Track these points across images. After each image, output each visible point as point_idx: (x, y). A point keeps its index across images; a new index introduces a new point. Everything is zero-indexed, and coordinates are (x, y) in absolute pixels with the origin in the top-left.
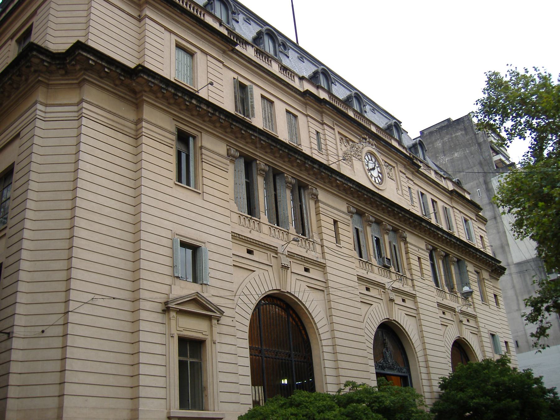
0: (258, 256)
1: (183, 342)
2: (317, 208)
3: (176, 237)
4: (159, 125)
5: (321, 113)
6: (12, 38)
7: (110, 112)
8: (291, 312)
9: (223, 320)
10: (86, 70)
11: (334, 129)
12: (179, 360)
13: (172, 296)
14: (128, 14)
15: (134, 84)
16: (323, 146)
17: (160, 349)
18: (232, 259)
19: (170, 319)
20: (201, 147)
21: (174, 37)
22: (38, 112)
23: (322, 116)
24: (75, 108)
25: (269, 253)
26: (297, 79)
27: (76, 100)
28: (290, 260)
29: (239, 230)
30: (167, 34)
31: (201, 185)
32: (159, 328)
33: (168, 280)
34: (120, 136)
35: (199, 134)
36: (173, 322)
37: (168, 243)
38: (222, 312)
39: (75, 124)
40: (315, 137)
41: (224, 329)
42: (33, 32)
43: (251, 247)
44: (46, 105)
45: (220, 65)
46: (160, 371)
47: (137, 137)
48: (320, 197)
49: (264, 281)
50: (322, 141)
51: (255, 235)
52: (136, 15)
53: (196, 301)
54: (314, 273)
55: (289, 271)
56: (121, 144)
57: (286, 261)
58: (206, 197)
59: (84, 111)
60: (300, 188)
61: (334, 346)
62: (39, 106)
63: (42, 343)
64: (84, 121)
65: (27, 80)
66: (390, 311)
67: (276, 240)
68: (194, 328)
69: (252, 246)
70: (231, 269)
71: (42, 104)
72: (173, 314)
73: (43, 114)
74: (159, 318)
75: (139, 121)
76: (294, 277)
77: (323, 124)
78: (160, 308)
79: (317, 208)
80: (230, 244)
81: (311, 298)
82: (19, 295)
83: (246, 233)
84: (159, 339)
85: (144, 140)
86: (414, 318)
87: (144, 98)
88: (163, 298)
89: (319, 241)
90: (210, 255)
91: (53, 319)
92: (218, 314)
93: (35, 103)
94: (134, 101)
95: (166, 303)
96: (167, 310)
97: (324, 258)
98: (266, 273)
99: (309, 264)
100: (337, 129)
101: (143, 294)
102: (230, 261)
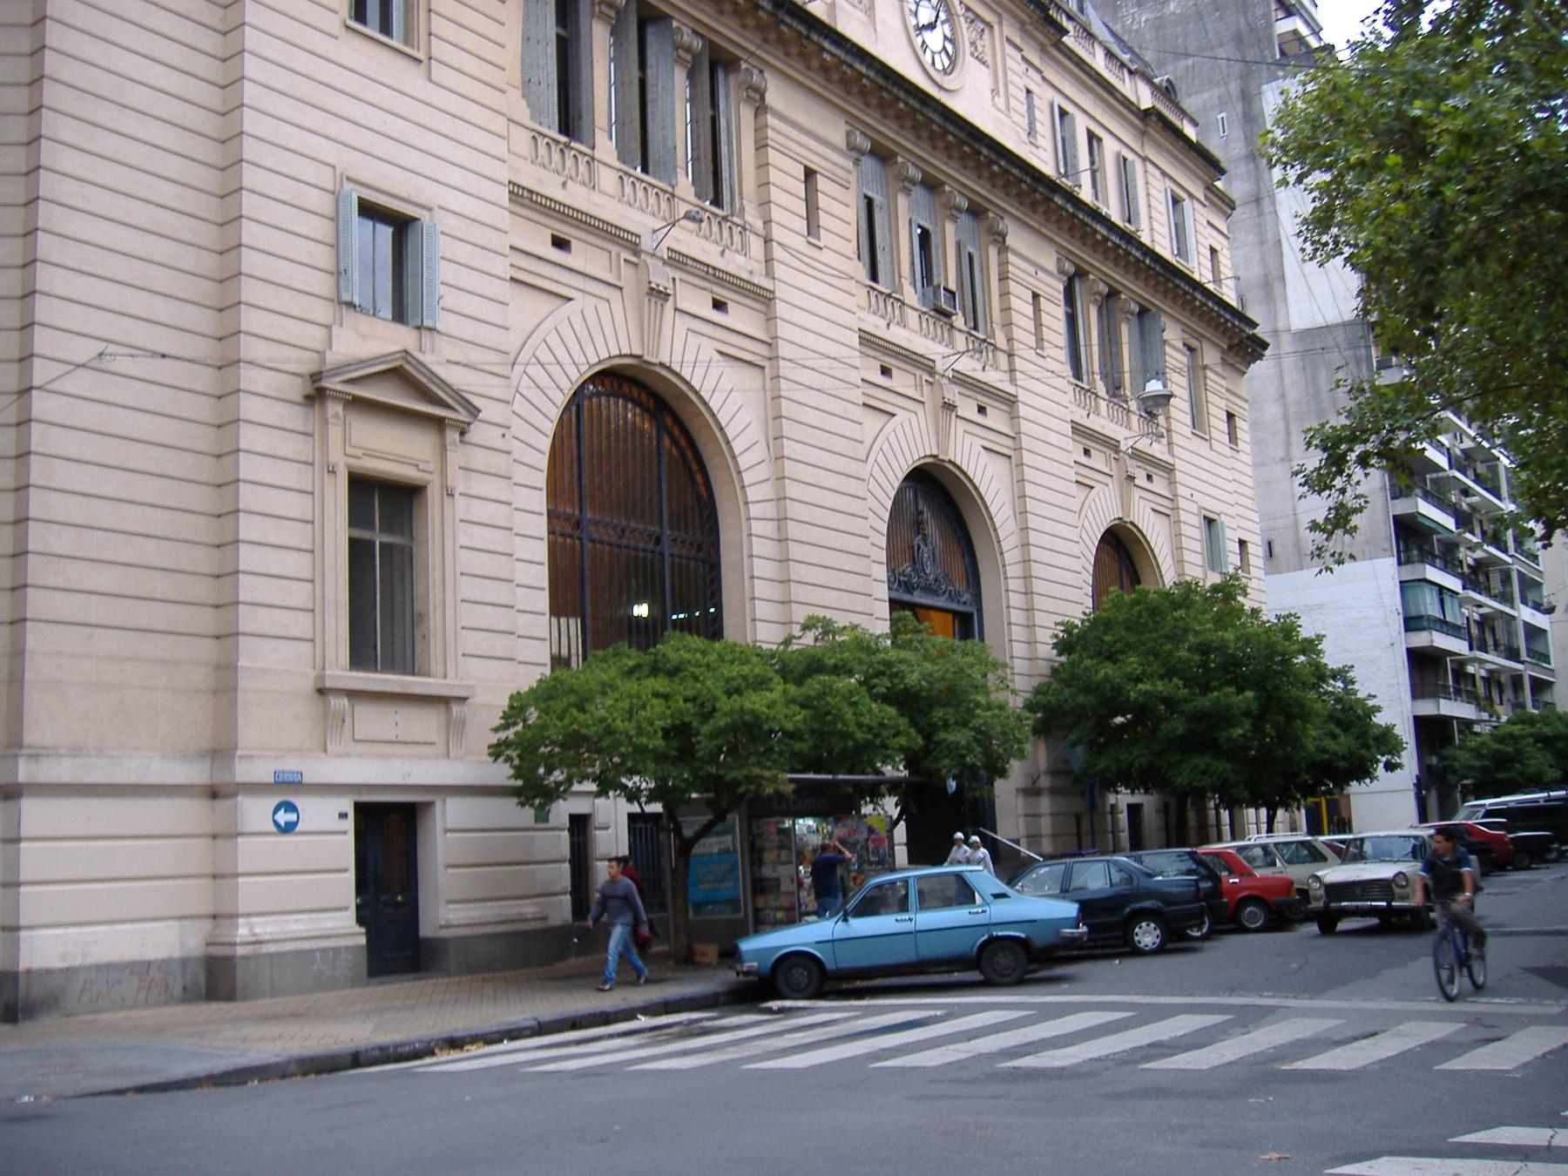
0: (583, 256)
3: (348, 186)
8: (669, 421)
9: (477, 433)
13: (332, 358)
17: (295, 505)
18: (507, 262)
25: (614, 249)
28: (672, 273)
29: (532, 178)
32: (294, 447)
36: (335, 432)
37: (324, 203)
38: (474, 411)
41: (480, 459)
43: (565, 231)
48: (771, 98)
51: (577, 197)
54: (740, 317)
55: (669, 305)
57: (661, 276)
66: (649, 329)
68: (395, 451)
69: (568, 228)
70: (505, 290)
72: (334, 408)
76: (683, 323)
78: (297, 389)
79: (760, 129)
80: (504, 219)
81: (726, 384)
83: (550, 187)
84: (292, 475)
86: (757, 371)
88: (307, 364)
92: (463, 416)
95: (316, 377)
96: (316, 395)
97: (769, 274)
98: (603, 307)
102: (502, 267)
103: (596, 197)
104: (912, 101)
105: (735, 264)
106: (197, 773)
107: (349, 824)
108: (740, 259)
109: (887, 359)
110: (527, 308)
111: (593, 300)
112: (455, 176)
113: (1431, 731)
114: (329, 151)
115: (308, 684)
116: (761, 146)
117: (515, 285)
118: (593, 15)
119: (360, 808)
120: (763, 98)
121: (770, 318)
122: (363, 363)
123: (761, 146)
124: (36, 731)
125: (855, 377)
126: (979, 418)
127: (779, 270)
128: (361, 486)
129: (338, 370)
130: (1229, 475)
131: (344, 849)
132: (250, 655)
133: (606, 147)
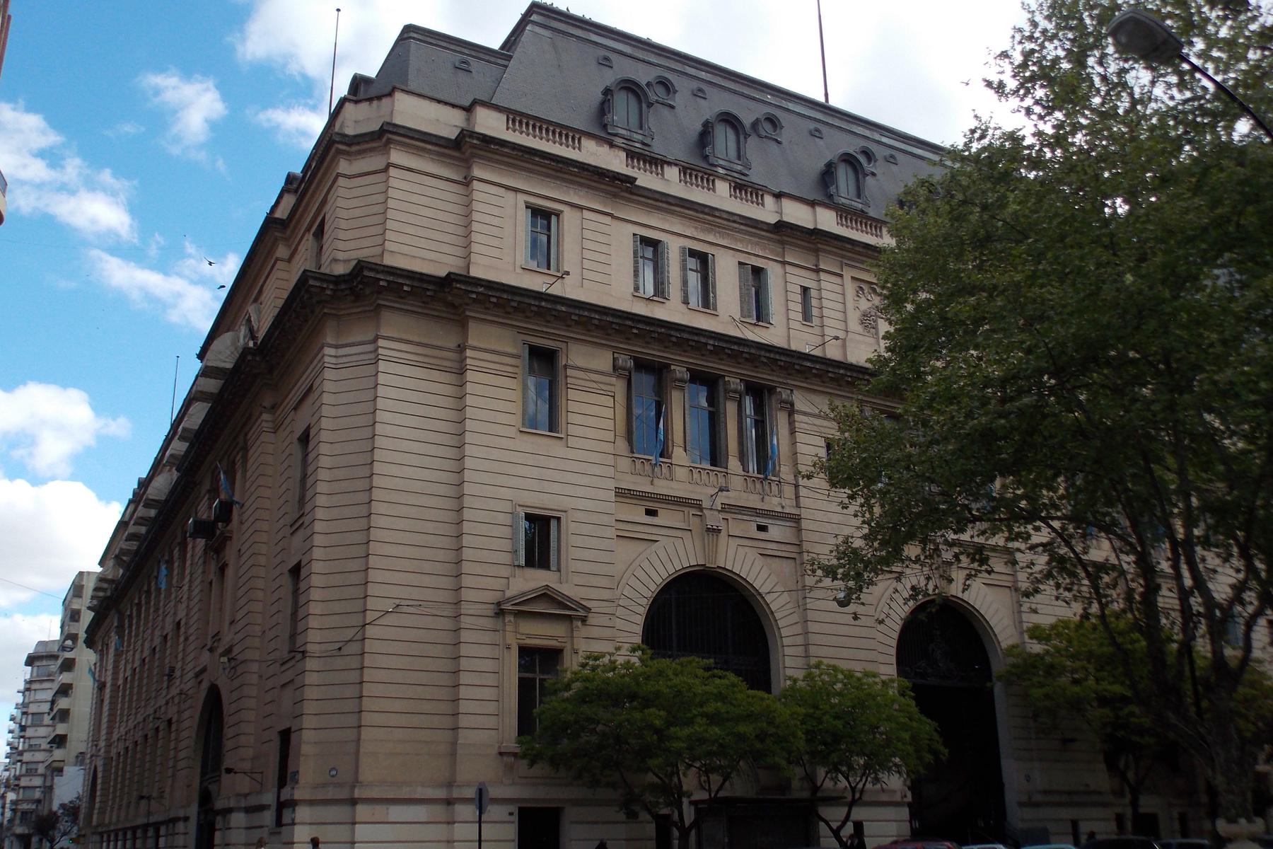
1: (528, 655)
2: (791, 423)
3: (519, 509)
4: (494, 350)
5: (816, 252)
6: (308, 230)
7: (418, 344)
9: (592, 620)
10: (379, 293)
11: (841, 276)
12: (520, 679)
13: (508, 594)
14: (447, 180)
15: (452, 299)
16: (815, 312)
17: (488, 665)
19: (505, 624)
20: (566, 367)
21: (522, 198)
22: (327, 359)
23: (817, 257)
24: (370, 347)
25: (686, 510)
26: (769, 200)
27: (371, 337)
29: (630, 482)
30: (511, 195)
31: (564, 425)
32: (488, 637)
33: (505, 571)
34: (436, 375)
35: (563, 346)
36: (509, 628)
37: (507, 519)
38: (588, 610)
39: (370, 370)
40: (799, 298)
41: (595, 632)
42: (326, 228)
43: (652, 505)
44: (336, 347)
45: (608, 220)
46: (488, 693)
47: (461, 371)
48: (799, 405)
49: (676, 554)
50: (814, 302)
51: (662, 487)
52: (460, 178)
53: (546, 595)
54: (777, 531)
56: (439, 385)
57: (713, 519)
58: (571, 441)
59: (380, 351)
60: (759, 392)
61: (806, 645)
62: (327, 351)
63: (339, 663)
64: (382, 366)
65: (312, 312)
67: (698, 489)
68: (542, 634)
69: (653, 505)
71: (331, 346)
72: (509, 618)
73: (333, 360)
74: (488, 623)
75: (461, 348)
76: (733, 543)
77: (817, 271)
78: (490, 610)
79: (791, 423)
80: (611, 508)
82: (312, 605)
83: (643, 485)
84: (486, 651)
85: (470, 375)
87: (468, 313)
88: (496, 597)
89: (791, 478)
90: (573, 527)
91: (349, 634)
92: (582, 613)
93: (322, 348)
94: (456, 318)
95: (499, 604)
96: (500, 613)
97: (798, 506)
98: (679, 543)
99: (763, 518)
100: (848, 273)
101: (467, 595)
102: (611, 533)
103: (674, 484)
104: (640, 326)
105: (773, 503)
106: (441, 793)
107: (515, 818)
108: (776, 500)
109: (651, 504)
110: (627, 551)
111: (672, 539)
112: (581, 492)
113: (598, 666)
114: (507, 493)
115: (495, 751)
116: (793, 432)
117: (621, 541)
118: (726, 399)
119: (520, 809)
120: (792, 405)
121: (799, 530)
122: (524, 594)
123: (793, 432)
124: (366, 774)
125: (611, 521)
126: (649, 519)
127: (803, 502)
128: (525, 652)
129: (509, 600)
130: (535, 472)
131: (511, 831)
132: (465, 737)
133: (734, 464)
